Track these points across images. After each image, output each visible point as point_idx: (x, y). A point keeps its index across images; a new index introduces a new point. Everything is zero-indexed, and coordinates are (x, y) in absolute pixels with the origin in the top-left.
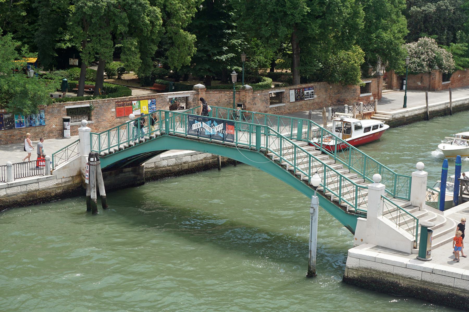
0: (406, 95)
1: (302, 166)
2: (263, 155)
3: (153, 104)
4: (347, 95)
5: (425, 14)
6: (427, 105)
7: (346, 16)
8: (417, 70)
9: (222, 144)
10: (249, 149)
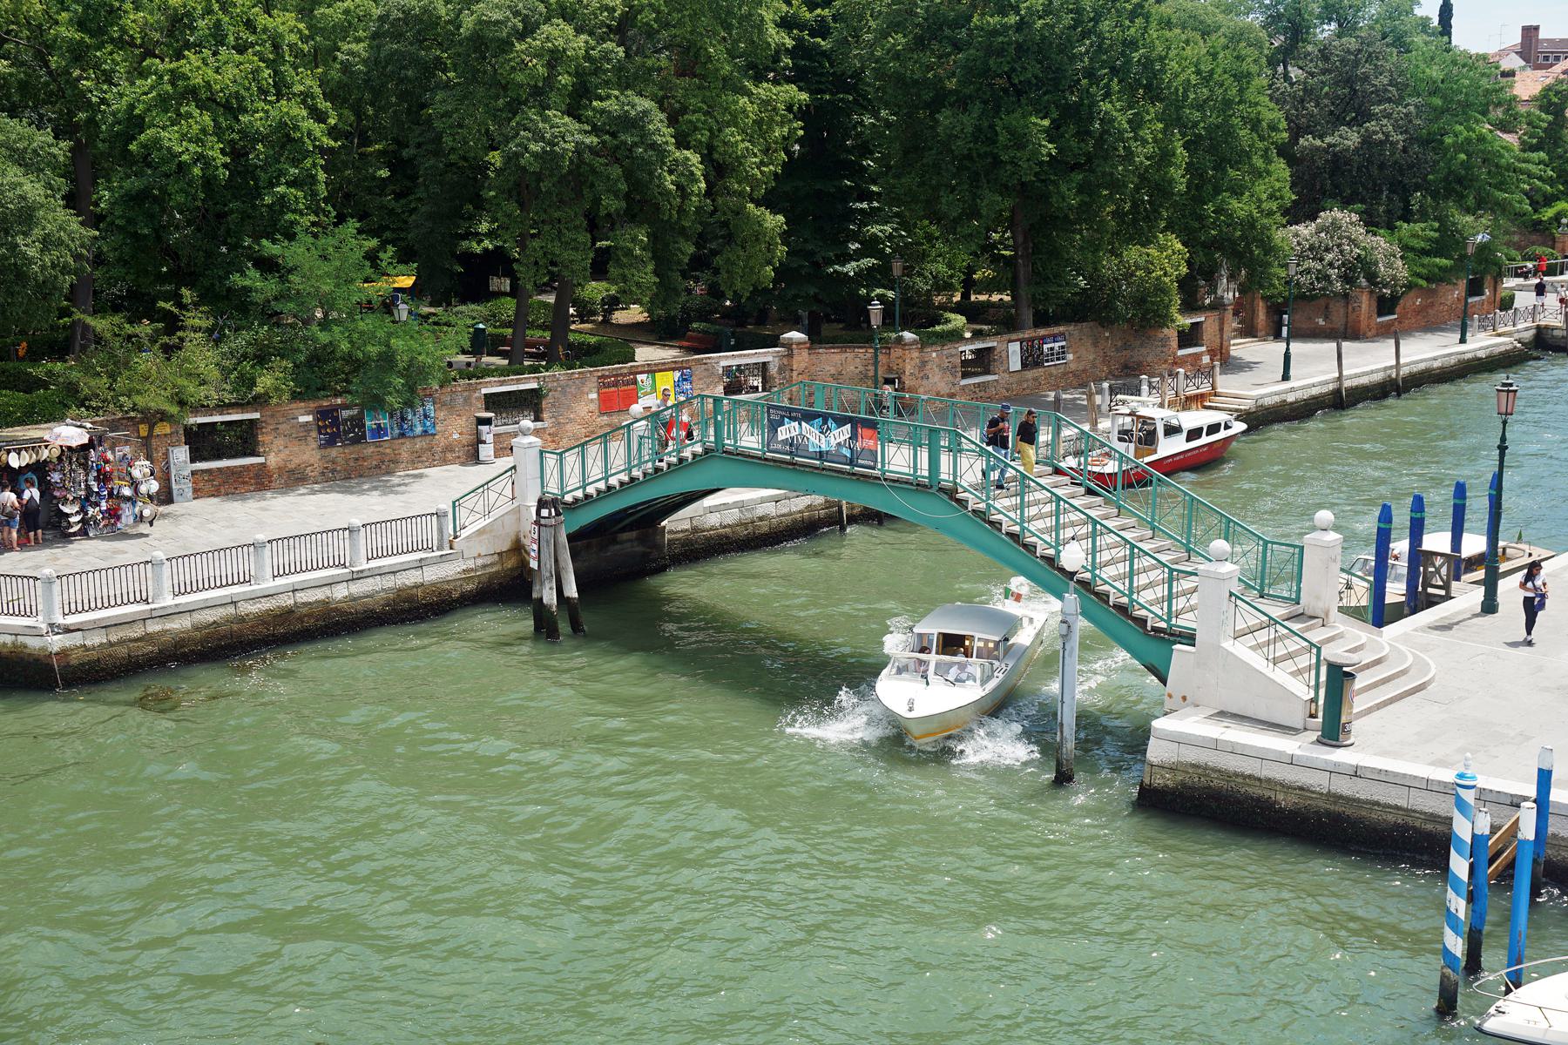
1: (1040, 524)
4: (1147, 354)
5: (1335, 155)
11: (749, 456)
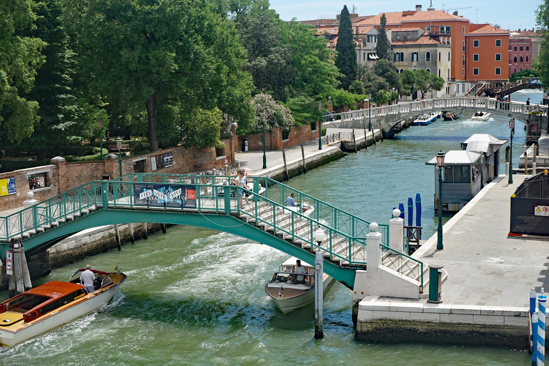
0: (264, 154)
1: (283, 224)
2: (234, 217)
3: (12, 183)
4: (203, 160)
5: (257, 70)
6: (285, 164)
7: (212, 72)
8: (258, 129)
9: (181, 212)
10: (215, 213)
11: (123, 208)
